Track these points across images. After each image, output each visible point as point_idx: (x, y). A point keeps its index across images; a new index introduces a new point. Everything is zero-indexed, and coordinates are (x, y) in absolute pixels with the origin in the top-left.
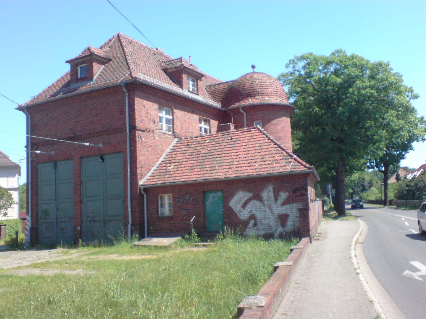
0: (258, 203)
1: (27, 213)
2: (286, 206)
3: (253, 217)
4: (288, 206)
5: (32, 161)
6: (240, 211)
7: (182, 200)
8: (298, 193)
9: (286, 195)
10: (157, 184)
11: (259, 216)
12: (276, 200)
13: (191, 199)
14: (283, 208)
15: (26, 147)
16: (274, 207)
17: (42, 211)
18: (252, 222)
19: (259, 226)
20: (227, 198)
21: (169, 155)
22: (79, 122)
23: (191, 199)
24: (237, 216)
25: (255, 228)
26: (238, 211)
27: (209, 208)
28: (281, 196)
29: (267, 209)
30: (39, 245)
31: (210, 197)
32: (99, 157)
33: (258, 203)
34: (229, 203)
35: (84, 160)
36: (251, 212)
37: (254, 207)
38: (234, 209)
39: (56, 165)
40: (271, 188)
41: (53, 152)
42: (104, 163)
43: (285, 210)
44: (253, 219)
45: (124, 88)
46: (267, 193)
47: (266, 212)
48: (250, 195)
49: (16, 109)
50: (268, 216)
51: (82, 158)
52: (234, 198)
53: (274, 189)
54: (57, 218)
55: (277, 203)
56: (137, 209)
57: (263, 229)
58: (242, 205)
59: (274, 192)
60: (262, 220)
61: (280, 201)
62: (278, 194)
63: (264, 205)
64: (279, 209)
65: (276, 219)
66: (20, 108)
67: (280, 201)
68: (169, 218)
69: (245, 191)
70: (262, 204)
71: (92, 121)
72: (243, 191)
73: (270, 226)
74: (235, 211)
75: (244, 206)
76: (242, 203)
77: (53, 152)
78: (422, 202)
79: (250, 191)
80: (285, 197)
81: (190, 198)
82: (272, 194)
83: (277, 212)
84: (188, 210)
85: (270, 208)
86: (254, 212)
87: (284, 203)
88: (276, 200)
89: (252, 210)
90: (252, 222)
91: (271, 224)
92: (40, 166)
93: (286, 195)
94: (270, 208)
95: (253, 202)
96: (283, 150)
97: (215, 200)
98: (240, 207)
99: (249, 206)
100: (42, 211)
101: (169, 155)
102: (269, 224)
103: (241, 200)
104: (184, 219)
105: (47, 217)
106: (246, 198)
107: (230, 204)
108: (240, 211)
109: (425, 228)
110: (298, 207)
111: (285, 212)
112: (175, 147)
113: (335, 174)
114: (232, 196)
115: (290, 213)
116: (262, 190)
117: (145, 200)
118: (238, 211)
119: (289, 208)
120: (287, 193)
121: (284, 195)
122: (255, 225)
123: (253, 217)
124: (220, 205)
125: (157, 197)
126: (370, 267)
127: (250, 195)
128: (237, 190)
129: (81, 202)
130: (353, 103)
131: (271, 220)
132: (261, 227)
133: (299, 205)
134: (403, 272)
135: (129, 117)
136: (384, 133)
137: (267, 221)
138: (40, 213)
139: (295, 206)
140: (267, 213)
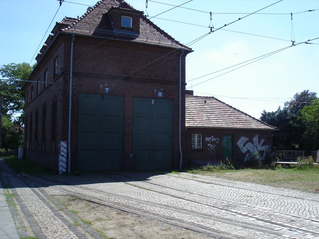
2: (264, 146)
4: (264, 147)
10: (197, 126)
16: (258, 147)
24: (241, 150)
33: (251, 144)
36: (248, 148)
37: (249, 146)
40: (257, 136)
48: (247, 139)
61: (261, 144)
63: (254, 145)
64: (260, 148)
67: (261, 144)
68: (197, 150)
75: (244, 145)
79: (247, 137)
87: (262, 145)
94: (257, 147)
96: (141, 188)
99: (247, 145)
107: (243, 137)
114: (239, 139)
121: (263, 141)
123: (248, 151)
124: (230, 143)
127: (247, 139)
134: (265, 141)
136: (291, 122)
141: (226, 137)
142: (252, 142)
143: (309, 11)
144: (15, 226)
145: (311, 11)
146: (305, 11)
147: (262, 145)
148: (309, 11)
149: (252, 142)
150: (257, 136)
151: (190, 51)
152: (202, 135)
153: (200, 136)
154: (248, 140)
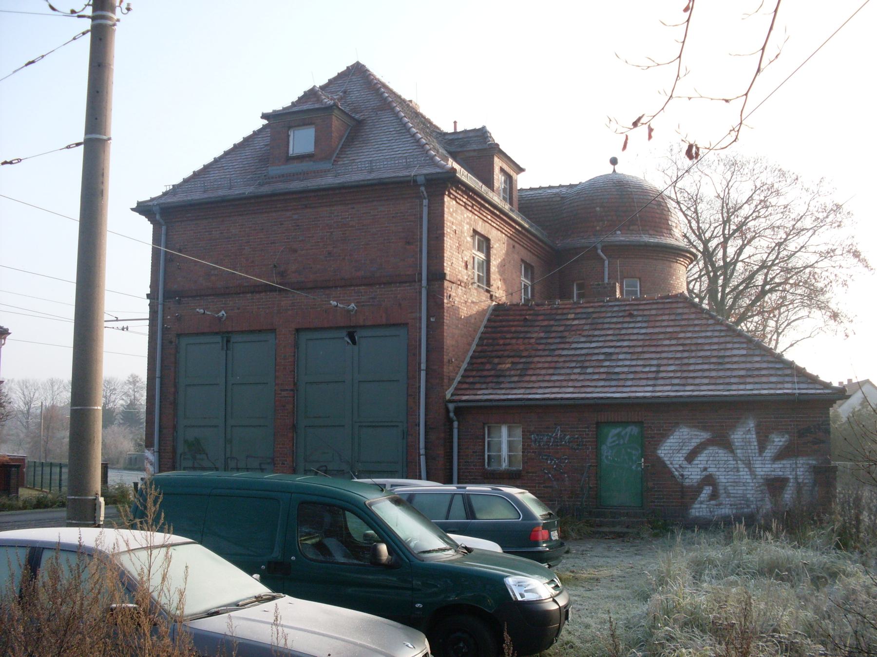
0: (722, 454)
1: (149, 444)
2: (784, 462)
3: (709, 480)
4: (786, 463)
5: (165, 330)
6: (681, 467)
7: (545, 439)
9: (783, 440)
11: (722, 479)
12: (762, 448)
13: (568, 437)
14: (774, 466)
15: (148, 296)
16: (757, 465)
17: (186, 441)
18: (707, 490)
19: (723, 498)
20: (648, 443)
21: (487, 339)
22: (295, 251)
23: (568, 437)
25: (713, 502)
26: (677, 466)
27: (607, 457)
28: (774, 442)
29: (741, 465)
30: (518, 482)
31: (611, 435)
32: (344, 334)
33: (722, 453)
34: (656, 449)
35: (304, 337)
36: (705, 469)
37: (712, 461)
38: (668, 462)
39: (228, 341)
40: (751, 424)
41: (223, 312)
42: (356, 348)
43: (780, 469)
44: (709, 485)
45: (423, 189)
46: (744, 434)
47: (738, 471)
48: (705, 436)
49: (133, 209)
50: (744, 481)
51: (298, 330)
52: (669, 441)
53: (758, 427)
54: (226, 459)
55: (764, 454)
56: (441, 451)
57: (731, 505)
58: (685, 455)
59: (757, 433)
60: (729, 488)
61: (769, 452)
62: (767, 437)
63: (736, 458)
64: (765, 467)
65: (759, 486)
66: (143, 209)
67: (769, 452)
69: (695, 427)
70: (730, 455)
71: (329, 253)
72: (690, 427)
73: (748, 500)
74: (670, 466)
75: (691, 457)
76: (685, 451)
77: (223, 312)
79: (704, 428)
80: (781, 444)
81: (565, 435)
82: (754, 436)
83: (762, 473)
84: (558, 459)
85: (749, 465)
86: (712, 470)
87: (780, 456)
88: (762, 448)
89: (707, 466)
90: (707, 490)
91: (748, 496)
93: (783, 440)
94: (749, 465)
95: (711, 450)
97: (622, 442)
98: (682, 459)
99: (702, 459)
100: (186, 441)
101: (487, 339)
102: (744, 496)
103: (684, 443)
105: (198, 456)
108: (681, 467)
110: (808, 464)
111: (781, 473)
112: (495, 322)
115: (791, 477)
116: (733, 427)
117: (455, 432)
118: (677, 466)
119: (789, 466)
121: (778, 441)
122: (714, 496)
123: (709, 480)
125: (484, 428)
127: (705, 436)
128: (677, 425)
129: (294, 427)
130: (598, 209)
131: (750, 488)
132: (727, 501)
133: (811, 462)
135: (429, 253)
137: (740, 490)
138: (181, 448)
139: (801, 462)
140: (741, 473)
141: (618, 430)
142: (728, 446)
143: (27, 65)
144: (669, 155)
145: (33, 62)
146: (15, 72)
147: (780, 456)
148: (27, 65)
149: (728, 446)
150: (752, 425)
151: (133, 209)
152: (484, 468)
153: (489, 465)
154: (708, 440)
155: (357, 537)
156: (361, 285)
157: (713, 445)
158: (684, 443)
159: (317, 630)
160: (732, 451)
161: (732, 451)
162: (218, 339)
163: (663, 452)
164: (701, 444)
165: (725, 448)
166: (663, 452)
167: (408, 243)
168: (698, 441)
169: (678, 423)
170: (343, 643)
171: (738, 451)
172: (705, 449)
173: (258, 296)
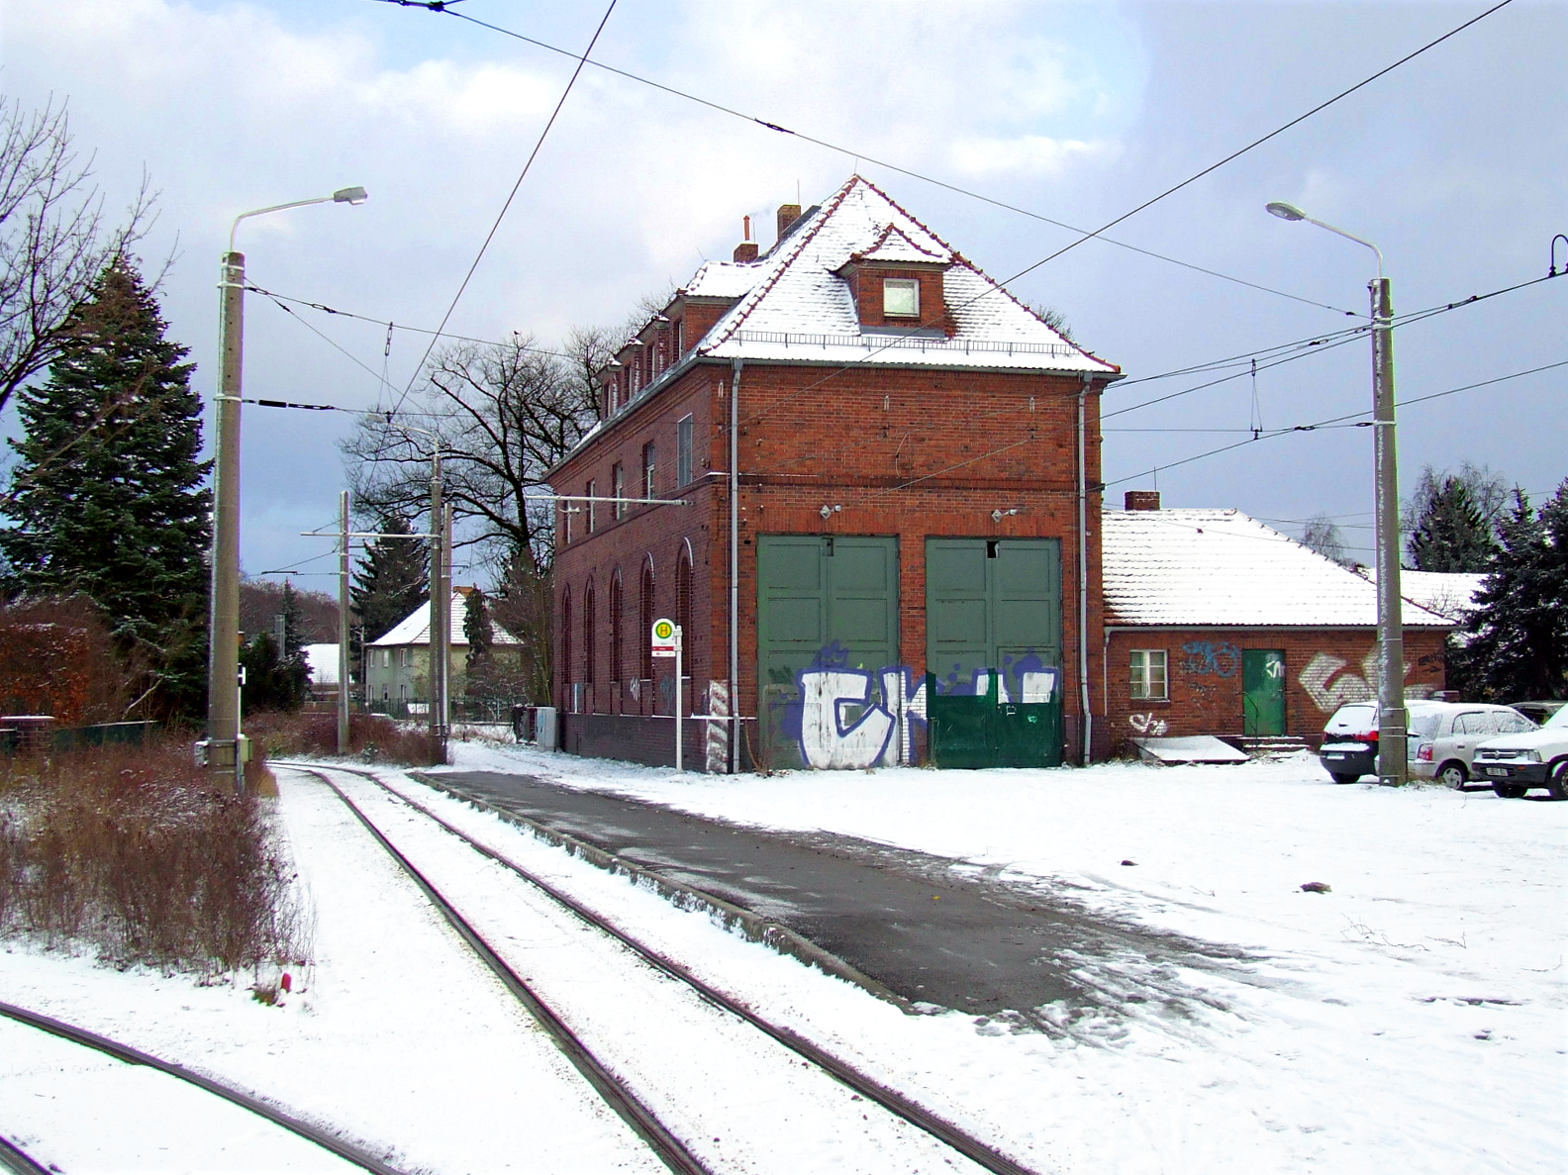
8: (1427, 666)
17: (771, 671)
20: (1292, 669)
34: (1297, 676)
35: (931, 543)
38: (1308, 690)
48: (1341, 663)
69: (1332, 654)
75: (1329, 684)
76: (1324, 679)
78: (1479, 613)
79: (1340, 656)
84: (1206, 687)
92: (764, 541)
95: (1345, 678)
103: (1323, 671)
104: (1197, 708)
106: (1332, 670)
109: (1526, 464)
113: (968, 998)
114: (1305, 663)
116: (1364, 656)
120: (283, 769)
126: (983, 1145)
127: (1341, 663)
142: (1360, 673)
149: (1360, 673)
154: (1343, 668)
155: (1129, 930)
156: (1006, 490)
157: (1348, 673)
158: (1323, 671)
159: (1350, 235)
160: (1364, 679)
161: (1364, 679)
162: (817, 540)
163: (1304, 679)
164: (1337, 672)
165: (1359, 676)
166: (1304, 679)
167: (1061, 446)
168: (1335, 668)
169: (1316, 651)
170: (1026, 655)
171: (1369, 678)
172: (1341, 676)
173: (873, 491)
